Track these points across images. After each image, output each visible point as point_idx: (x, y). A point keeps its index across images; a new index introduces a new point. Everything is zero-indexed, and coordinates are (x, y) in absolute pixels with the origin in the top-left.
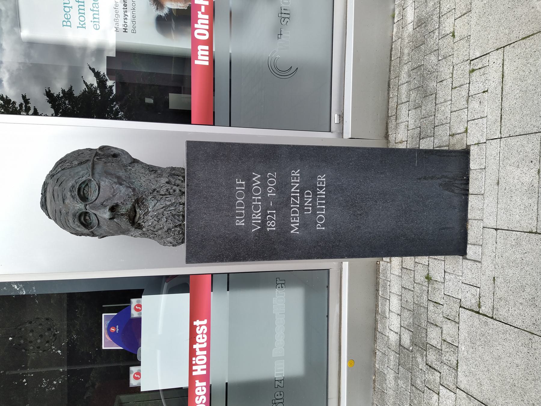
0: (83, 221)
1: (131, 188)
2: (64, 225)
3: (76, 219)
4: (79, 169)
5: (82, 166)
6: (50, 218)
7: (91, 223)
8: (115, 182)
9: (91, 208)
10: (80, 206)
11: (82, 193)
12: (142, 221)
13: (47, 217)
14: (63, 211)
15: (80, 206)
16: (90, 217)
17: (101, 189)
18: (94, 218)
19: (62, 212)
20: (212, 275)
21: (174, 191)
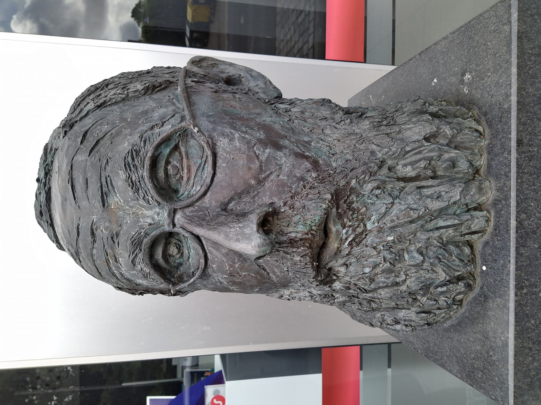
0: (161, 261)
1: (307, 158)
2: (102, 269)
3: (140, 256)
4: (149, 103)
5: (155, 96)
6: (60, 247)
7: (181, 264)
8: (260, 141)
9: (190, 220)
10: (154, 215)
11: (161, 174)
12: (341, 261)
13: (54, 245)
14: (102, 232)
15: (154, 215)
16: (179, 248)
17: (219, 162)
18: (192, 250)
19: (98, 233)
20: (361, 346)
21: (453, 164)
